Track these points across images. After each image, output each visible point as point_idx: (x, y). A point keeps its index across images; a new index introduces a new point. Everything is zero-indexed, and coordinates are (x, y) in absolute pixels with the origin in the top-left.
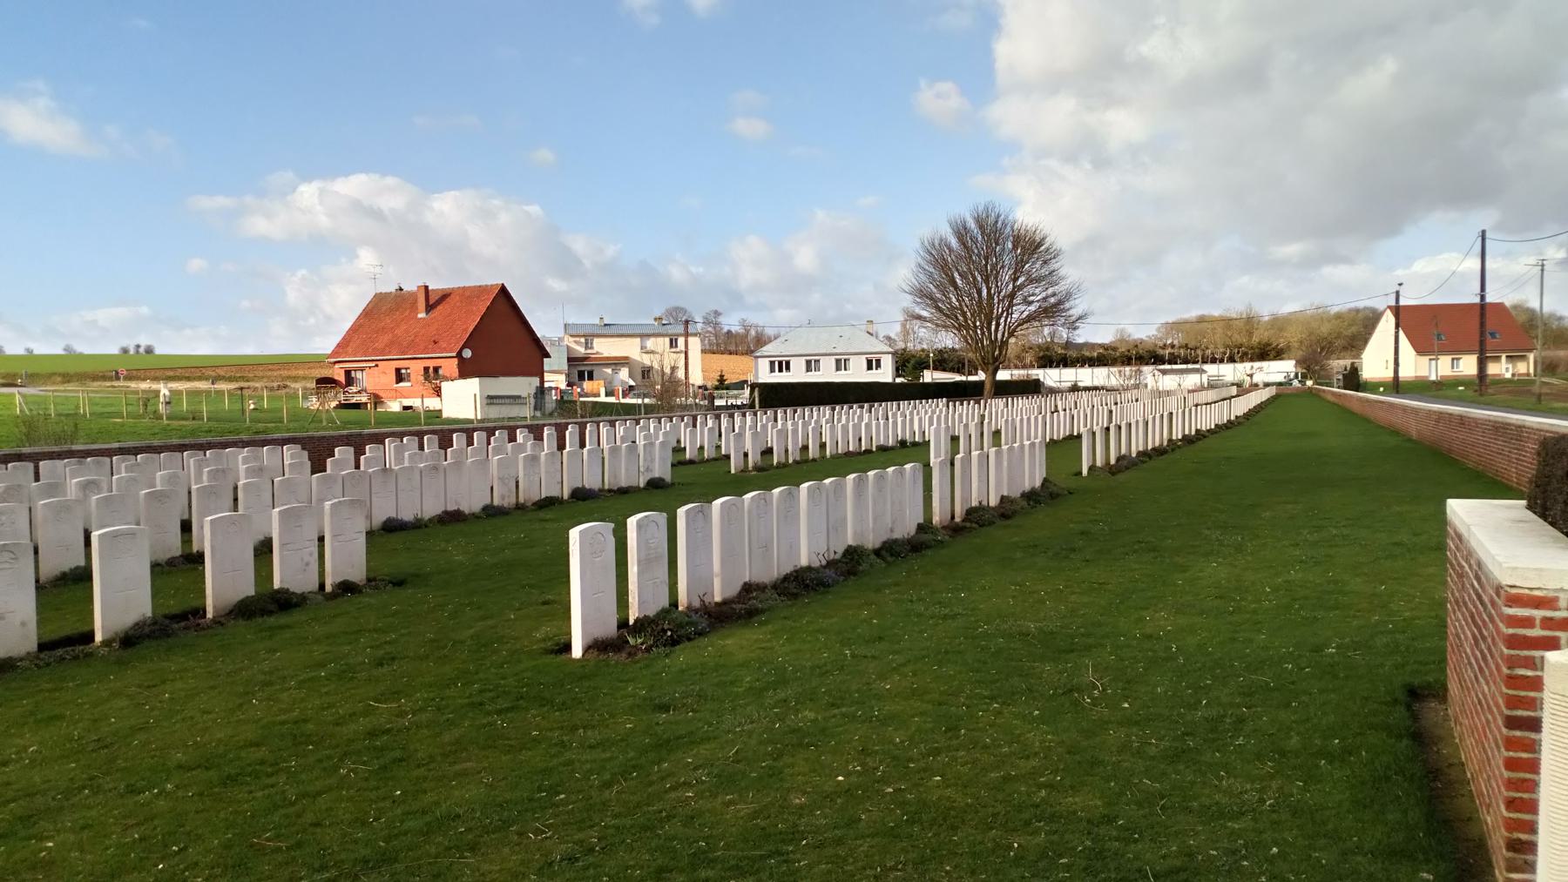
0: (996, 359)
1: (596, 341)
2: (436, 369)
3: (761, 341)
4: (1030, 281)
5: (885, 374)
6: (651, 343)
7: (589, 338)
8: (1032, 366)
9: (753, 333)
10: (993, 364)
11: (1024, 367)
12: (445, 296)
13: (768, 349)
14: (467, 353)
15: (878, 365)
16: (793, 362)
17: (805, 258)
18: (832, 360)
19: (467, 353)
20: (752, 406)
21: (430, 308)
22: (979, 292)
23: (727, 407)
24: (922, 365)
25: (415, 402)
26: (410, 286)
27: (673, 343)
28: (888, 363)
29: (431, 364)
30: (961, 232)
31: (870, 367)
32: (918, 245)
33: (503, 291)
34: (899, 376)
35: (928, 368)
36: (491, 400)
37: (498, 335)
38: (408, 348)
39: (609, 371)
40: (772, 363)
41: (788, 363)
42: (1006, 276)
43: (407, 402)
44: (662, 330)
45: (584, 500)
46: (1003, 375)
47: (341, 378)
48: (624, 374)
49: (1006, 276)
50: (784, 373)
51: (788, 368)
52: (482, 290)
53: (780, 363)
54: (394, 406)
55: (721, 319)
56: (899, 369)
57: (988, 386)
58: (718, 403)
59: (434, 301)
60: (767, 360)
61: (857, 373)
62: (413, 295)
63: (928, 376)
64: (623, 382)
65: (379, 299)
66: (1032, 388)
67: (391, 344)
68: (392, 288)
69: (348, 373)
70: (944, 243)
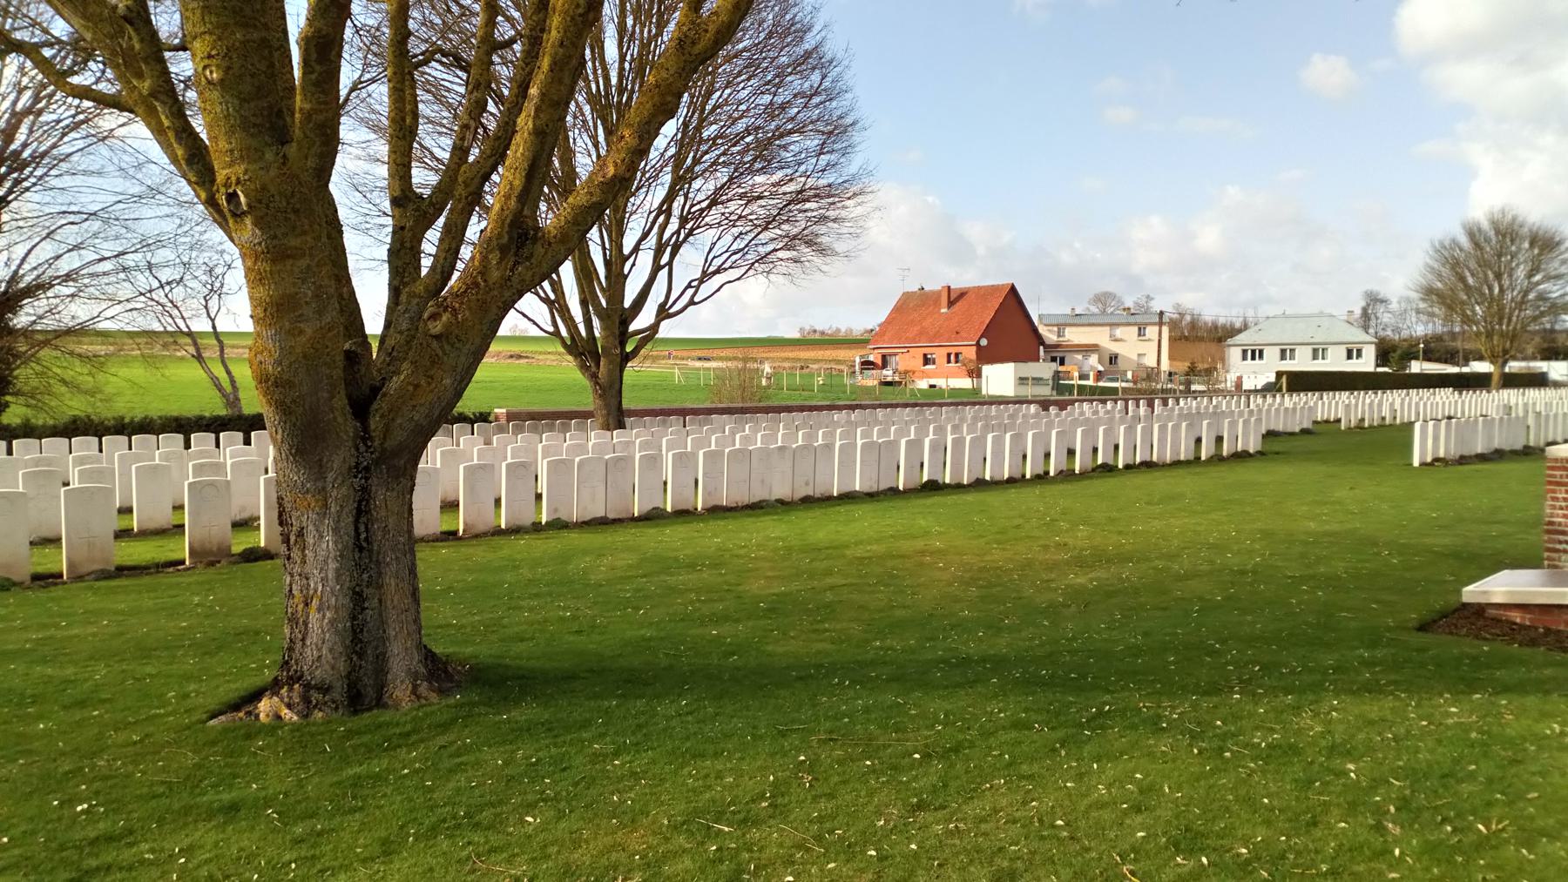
0: (1505, 352)
1: (1068, 330)
2: (957, 355)
3: (1232, 332)
4: (1547, 278)
5: (1367, 363)
6: (1119, 332)
7: (1061, 327)
8: (1534, 358)
9: (1188, 318)
10: (1500, 357)
11: (1524, 359)
12: (962, 294)
13: (1241, 338)
14: (984, 342)
15: (1359, 354)
16: (1299, 350)
17: (1209, 238)
18: (1277, 350)
19: (984, 342)
20: (1280, 390)
21: (951, 304)
22: (1491, 288)
23: (1163, 391)
24: (1411, 355)
25: (941, 382)
26: (933, 286)
27: (1141, 333)
28: (1370, 353)
29: (953, 350)
30: (1473, 234)
31: (1349, 357)
32: (1427, 245)
33: (1013, 289)
34: (1378, 365)
35: (1417, 358)
36: (1022, 380)
37: (1008, 327)
38: (935, 337)
39: (1080, 357)
40: (1245, 352)
41: (1261, 352)
42: (1521, 273)
43: (933, 382)
44: (1132, 319)
45: (256, 560)
46: (1514, 366)
47: (879, 362)
48: (1093, 360)
49: (1521, 273)
50: (1320, 361)
51: (1261, 356)
52: (994, 289)
53: (1253, 352)
54: (923, 384)
55: (1152, 304)
56: (1384, 355)
57: (1495, 379)
58: (1193, 387)
59: (955, 297)
60: (1310, 348)
61: (1335, 362)
62: (938, 293)
63: (1416, 367)
64: (1092, 368)
65: (907, 297)
66: (1540, 381)
67: (920, 333)
68: (915, 288)
69: (884, 357)
70: (1454, 242)
